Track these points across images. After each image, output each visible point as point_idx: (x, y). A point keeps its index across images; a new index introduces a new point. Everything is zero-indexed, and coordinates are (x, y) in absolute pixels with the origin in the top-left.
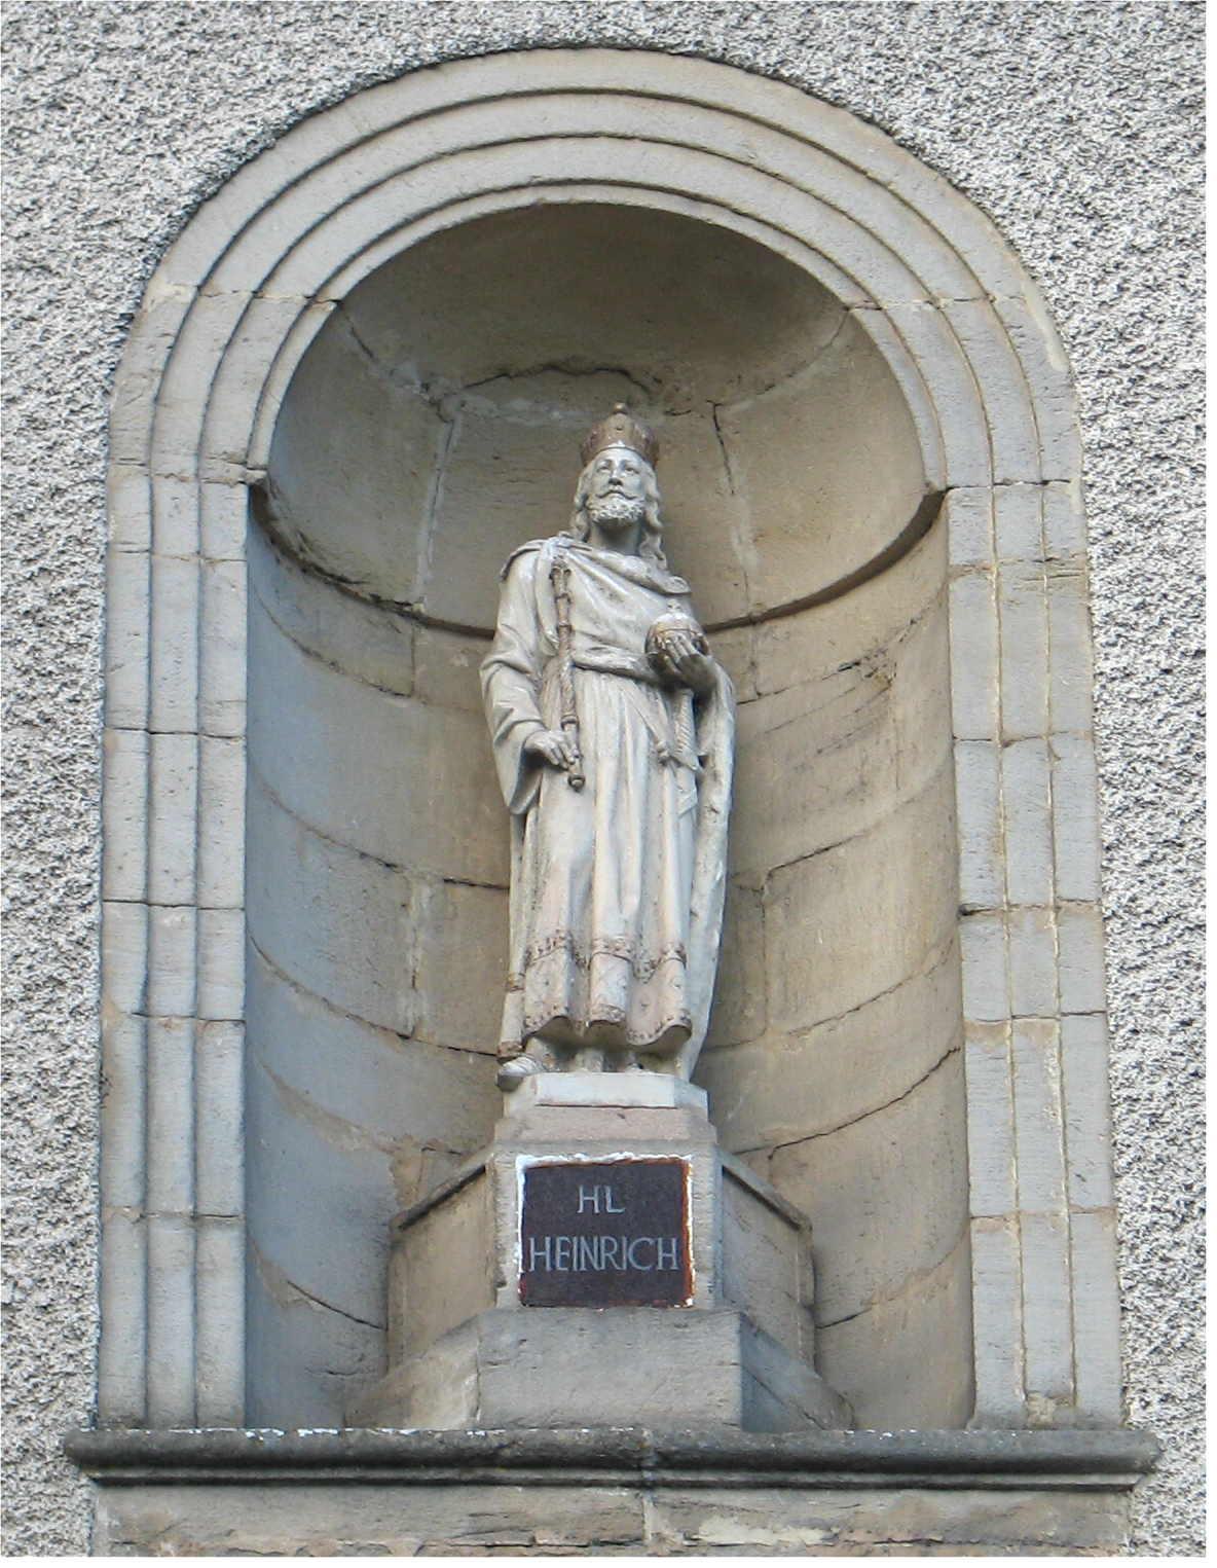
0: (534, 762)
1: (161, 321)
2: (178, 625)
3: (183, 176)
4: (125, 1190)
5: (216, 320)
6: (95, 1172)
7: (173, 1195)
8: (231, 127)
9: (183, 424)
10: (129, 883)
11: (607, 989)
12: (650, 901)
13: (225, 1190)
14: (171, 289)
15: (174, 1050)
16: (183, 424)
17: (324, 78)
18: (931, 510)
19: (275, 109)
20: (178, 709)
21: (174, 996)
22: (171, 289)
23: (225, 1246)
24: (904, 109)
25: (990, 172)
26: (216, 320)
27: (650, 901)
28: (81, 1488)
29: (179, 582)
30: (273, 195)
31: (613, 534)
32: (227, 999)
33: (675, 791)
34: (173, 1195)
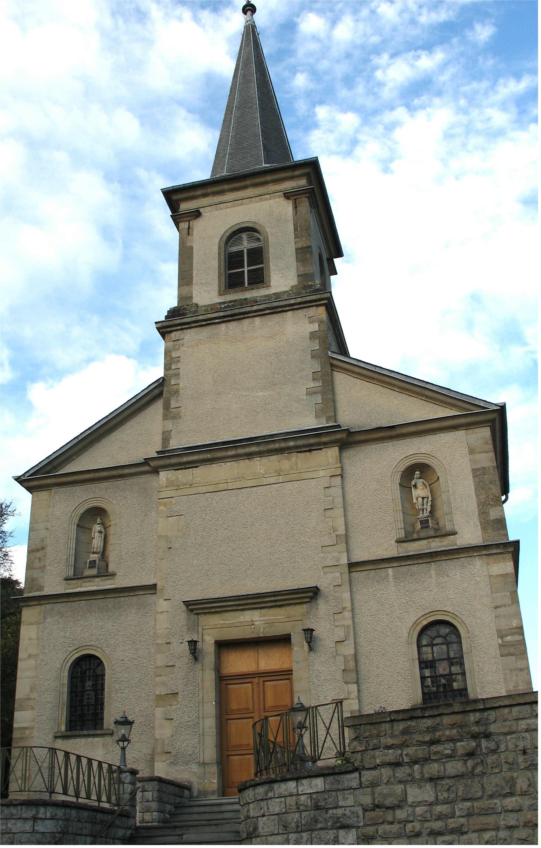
0: (93, 538)
1: (73, 516)
2: (72, 533)
3: (74, 508)
4: (68, 564)
5: (75, 516)
6: (384, 711)
7: (70, 564)
8: (76, 505)
9: (73, 522)
10: (69, 548)
11: (95, 550)
12: (98, 546)
13: (73, 564)
14: (73, 514)
15: (71, 556)
16: (73, 522)
17: (81, 502)
18: (439, 477)
19: (79, 504)
20: (72, 538)
21: (71, 554)
22: (73, 514)
23: (73, 567)
24: (110, 499)
25: (114, 502)
26: (75, 516)
27: (98, 546)
28: (65, 581)
29: (73, 531)
30: (183, 470)
31: (98, 524)
32: (74, 553)
33: (100, 538)
34: (70, 564)
